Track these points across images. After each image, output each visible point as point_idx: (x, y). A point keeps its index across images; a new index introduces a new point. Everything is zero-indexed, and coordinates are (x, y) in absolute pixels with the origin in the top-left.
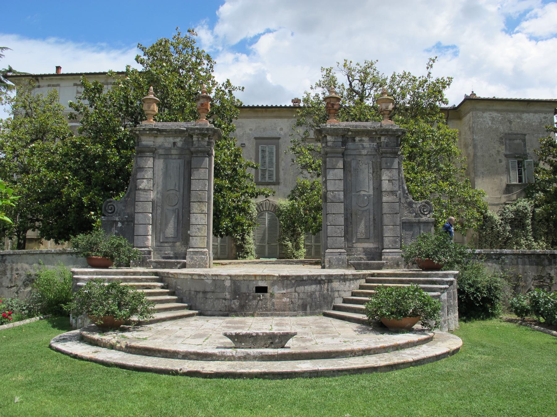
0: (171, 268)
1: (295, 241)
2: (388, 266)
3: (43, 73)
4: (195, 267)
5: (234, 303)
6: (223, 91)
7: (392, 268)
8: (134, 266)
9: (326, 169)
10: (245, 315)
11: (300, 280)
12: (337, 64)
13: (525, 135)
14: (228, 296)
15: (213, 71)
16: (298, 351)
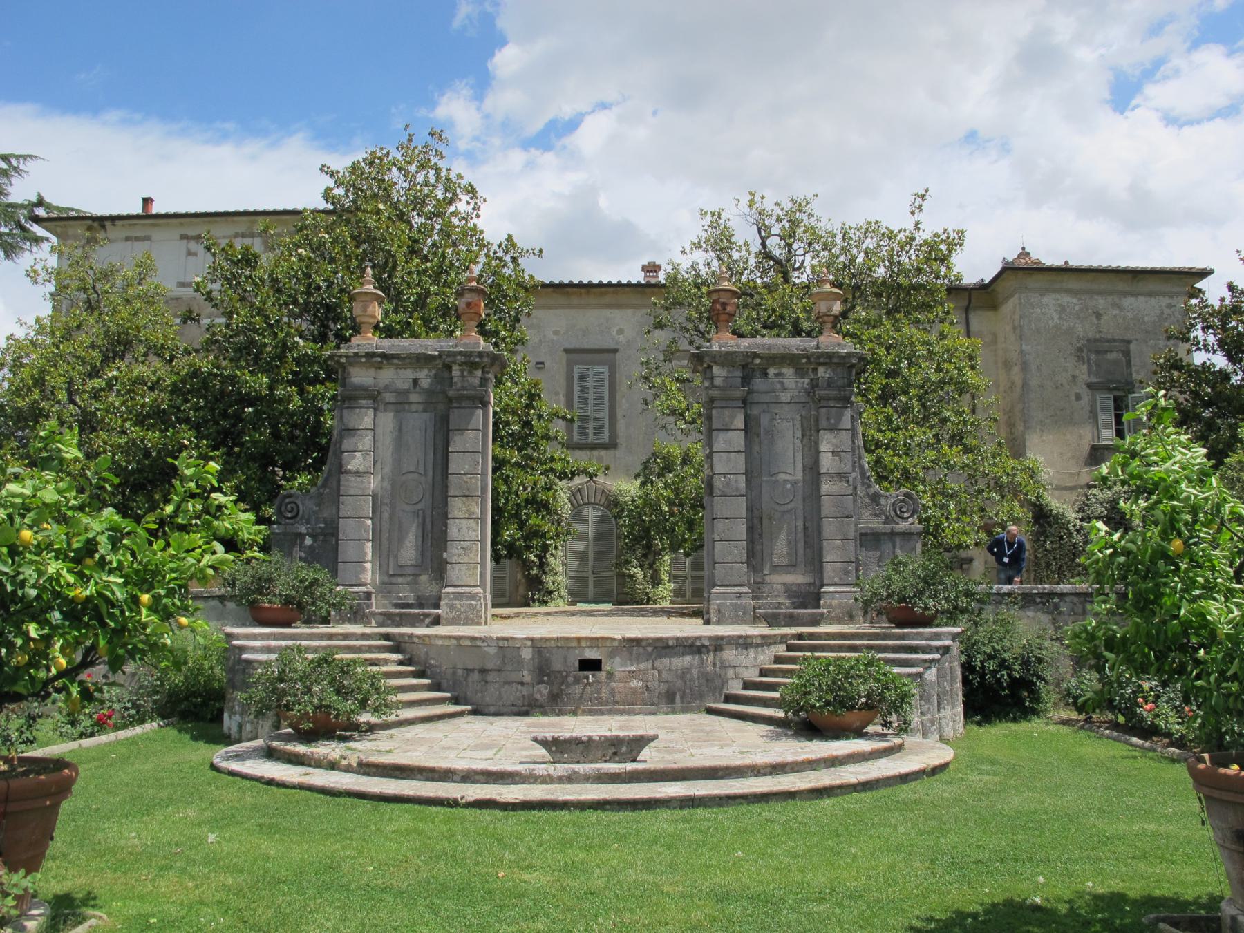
0: (413, 625)
1: (651, 566)
2: (832, 618)
3: (115, 213)
4: (458, 624)
5: (539, 691)
6: (501, 259)
7: (839, 621)
8: (338, 622)
9: (710, 430)
10: (560, 713)
11: (662, 647)
12: (734, 203)
13: (1129, 342)
14: (527, 678)
15: (478, 216)
16: (661, 766)
